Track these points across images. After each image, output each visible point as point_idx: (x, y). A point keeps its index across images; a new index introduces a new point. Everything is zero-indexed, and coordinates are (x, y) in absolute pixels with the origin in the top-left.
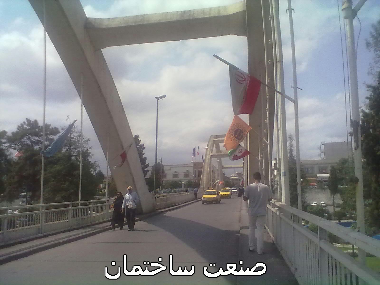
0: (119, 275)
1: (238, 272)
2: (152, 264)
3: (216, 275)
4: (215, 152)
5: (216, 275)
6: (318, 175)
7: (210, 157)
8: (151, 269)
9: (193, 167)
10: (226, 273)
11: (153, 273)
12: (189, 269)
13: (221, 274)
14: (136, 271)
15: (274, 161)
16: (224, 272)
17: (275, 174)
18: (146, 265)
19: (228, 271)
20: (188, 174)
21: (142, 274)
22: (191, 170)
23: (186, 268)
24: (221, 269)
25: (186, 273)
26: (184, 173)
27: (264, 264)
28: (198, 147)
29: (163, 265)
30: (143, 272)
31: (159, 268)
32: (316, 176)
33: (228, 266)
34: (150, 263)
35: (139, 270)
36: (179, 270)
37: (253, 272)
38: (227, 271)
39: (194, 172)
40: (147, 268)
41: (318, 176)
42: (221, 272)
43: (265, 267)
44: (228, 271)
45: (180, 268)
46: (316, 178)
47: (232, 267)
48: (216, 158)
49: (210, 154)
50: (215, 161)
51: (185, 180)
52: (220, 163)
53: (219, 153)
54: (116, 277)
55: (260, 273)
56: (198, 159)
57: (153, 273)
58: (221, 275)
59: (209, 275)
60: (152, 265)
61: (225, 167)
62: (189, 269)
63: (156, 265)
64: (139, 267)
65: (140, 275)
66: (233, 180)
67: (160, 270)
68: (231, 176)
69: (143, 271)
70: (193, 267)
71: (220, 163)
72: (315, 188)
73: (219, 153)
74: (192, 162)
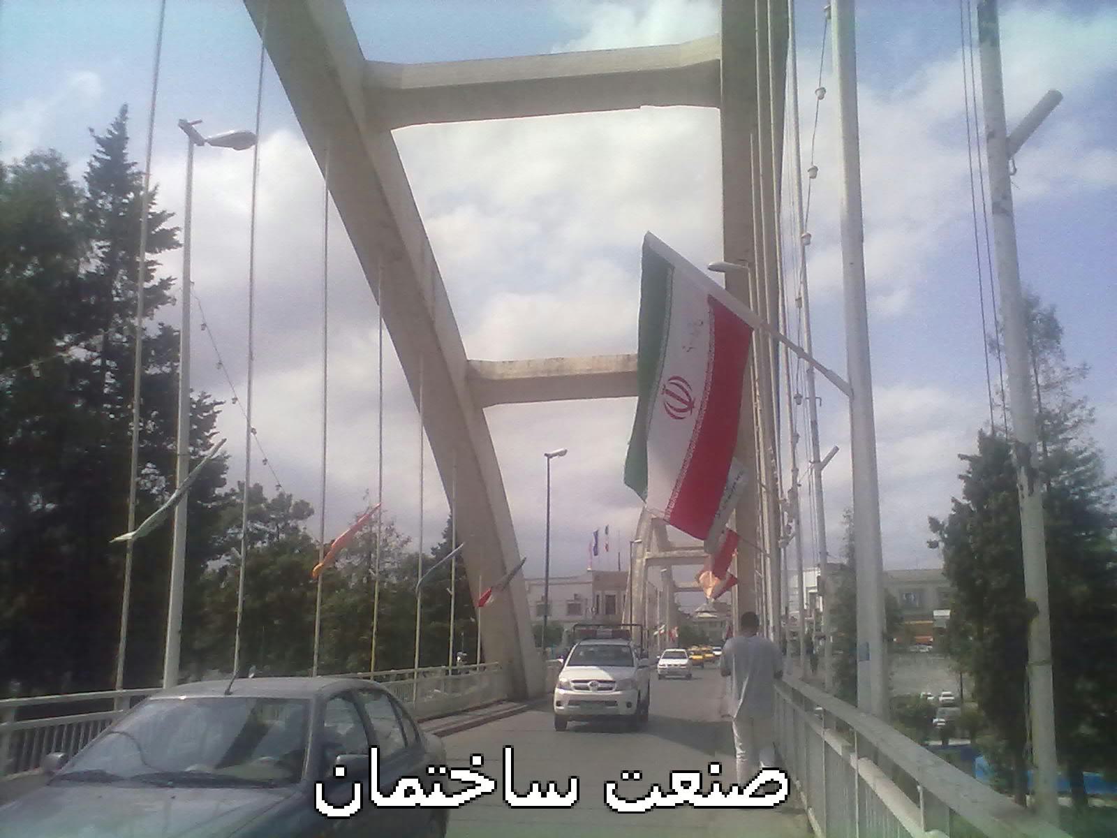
0: (355, 806)
1: (705, 796)
2: (453, 772)
3: (641, 806)
4: (655, 552)
5: (641, 806)
6: (936, 613)
7: (644, 564)
8: (452, 787)
9: (591, 585)
10: (670, 801)
11: (455, 801)
12: (563, 789)
13: (655, 804)
14: (407, 795)
15: (816, 572)
16: (664, 796)
17: (819, 609)
18: (435, 778)
19: (677, 793)
20: (579, 605)
21: (425, 801)
22: (586, 592)
23: (552, 786)
24: (656, 788)
25: (553, 799)
26: (569, 601)
27: (783, 775)
28: (607, 528)
29: (485, 777)
30: (427, 796)
31: (473, 785)
32: (933, 614)
33: (677, 778)
34: (448, 772)
35: (413, 792)
36: (532, 791)
37: (750, 796)
38: (674, 793)
39: (594, 599)
40: (437, 786)
41: (937, 616)
42: (656, 798)
43: (784, 782)
44: (677, 793)
45: (535, 786)
46: (932, 622)
47: (689, 783)
48: (659, 567)
49: (643, 557)
50: (656, 574)
51: (569, 622)
52: (668, 576)
53: (668, 553)
54: (346, 812)
55: (769, 800)
56: (607, 563)
57: (455, 801)
58: (655, 806)
59: (622, 806)
60: (453, 777)
61: (680, 587)
62: (563, 789)
63: (465, 775)
64: (414, 783)
65: (418, 805)
66: (703, 622)
67: (478, 791)
68: (697, 612)
69: (427, 793)
70: (574, 782)
71: (668, 576)
72: (927, 650)
73: (668, 554)
74: (589, 571)
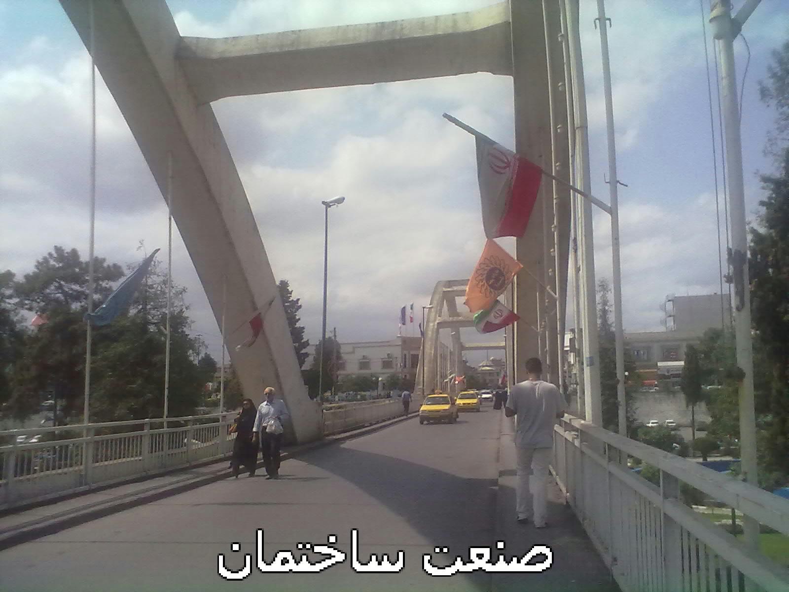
0: (247, 571)
1: (494, 564)
2: (315, 547)
3: (448, 571)
4: (446, 316)
5: (448, 571)
6: (660, 364)
7: (436, 327)
8: (313, 558)
9: (400, 347)
10: (469, 568)
11: (318, 567)
12: (393, 559)
13: (458, 570)
14: (283, 564)
15: (570, 335)
16: (464, 564)
17: (570, 362)
18: (304, 551)
19: (474, 562)
20: (391, 361)
21: (296, 568)
22: (397, 352)
23: (385, 557)
24: (459, 559)
25: (386, 566)
26: (383, 359)
27: (549, 549)
28: (412, 305)
29: (338, 551)
30: (297, 565)
31: (330, 556)
32: (657, 365)
33: (474, 552)
34: (312, 547)
35: (288, 562)
36: (371, 561)
37: (526, 564)
38: (472, 562)
39: (402, 357)
40: (304, 557)
41: (660, 366)
42: (459, 565)
43: (550, 555)
44: (474, 562)
45: (374, 557)
46: (656, 370)
47: (482, 555)
48: (449, 329)
49: (435, 320)
50: (446, 335)
51: (383, 373)
52: (457, 338)
53: (455, 318)
54: (240, 575)
55: (539, 567)
56: (412, 331)
57: (318, 567)
58: (458, 571)
59: (435, 571)
60: (315, 551)
61: (467, 346)
62: (393, 559)
63: (324, 550)
64: (288, 555)
65: (291, 570)
66: (484, 373)
67: (333, 561)
68: (480, 366)
69: (297, 563)
70: (401, 554)
71: (457, 338)
72: (654, 391)
73: (455, 319)
74: (398, 337)
